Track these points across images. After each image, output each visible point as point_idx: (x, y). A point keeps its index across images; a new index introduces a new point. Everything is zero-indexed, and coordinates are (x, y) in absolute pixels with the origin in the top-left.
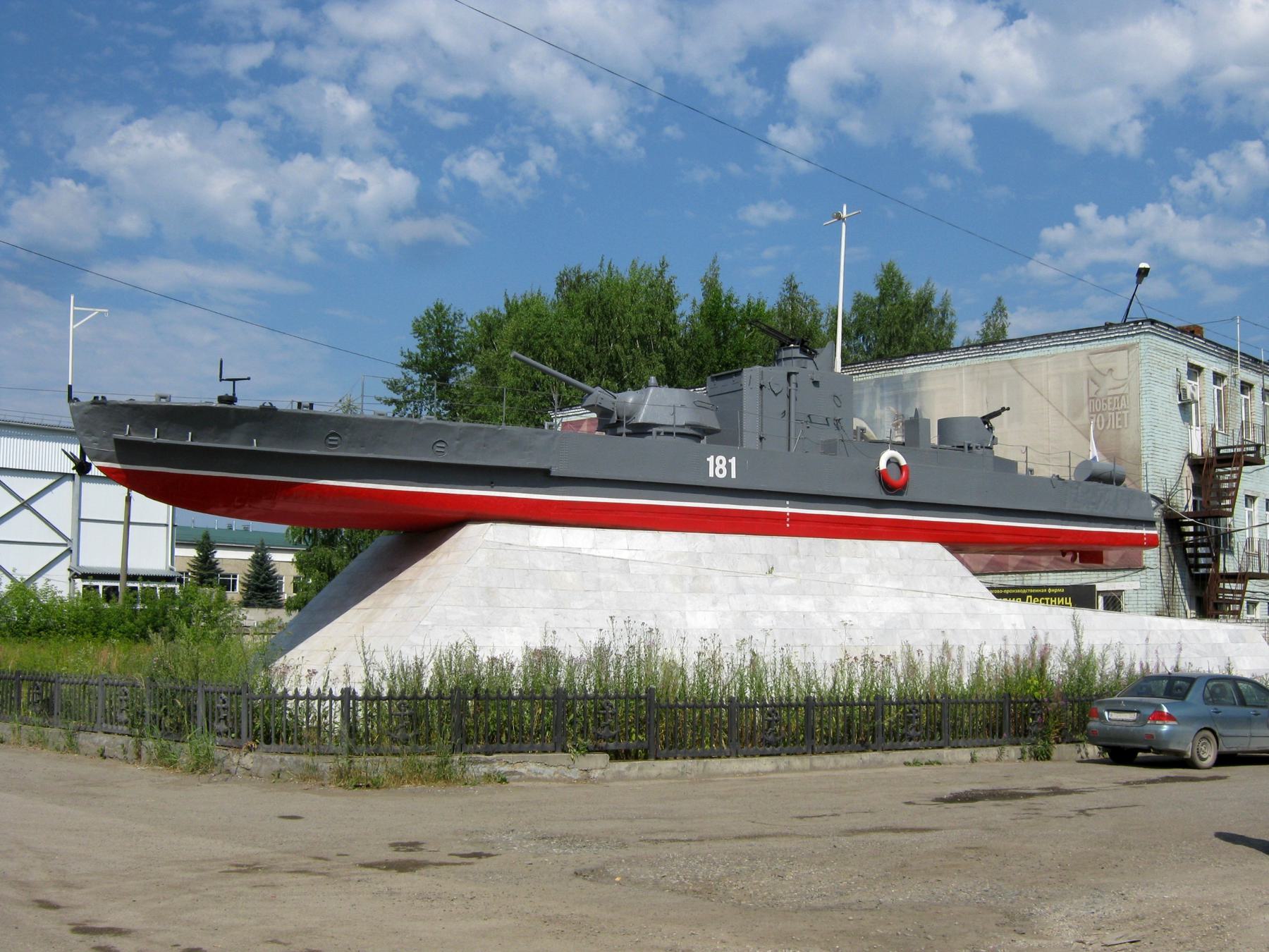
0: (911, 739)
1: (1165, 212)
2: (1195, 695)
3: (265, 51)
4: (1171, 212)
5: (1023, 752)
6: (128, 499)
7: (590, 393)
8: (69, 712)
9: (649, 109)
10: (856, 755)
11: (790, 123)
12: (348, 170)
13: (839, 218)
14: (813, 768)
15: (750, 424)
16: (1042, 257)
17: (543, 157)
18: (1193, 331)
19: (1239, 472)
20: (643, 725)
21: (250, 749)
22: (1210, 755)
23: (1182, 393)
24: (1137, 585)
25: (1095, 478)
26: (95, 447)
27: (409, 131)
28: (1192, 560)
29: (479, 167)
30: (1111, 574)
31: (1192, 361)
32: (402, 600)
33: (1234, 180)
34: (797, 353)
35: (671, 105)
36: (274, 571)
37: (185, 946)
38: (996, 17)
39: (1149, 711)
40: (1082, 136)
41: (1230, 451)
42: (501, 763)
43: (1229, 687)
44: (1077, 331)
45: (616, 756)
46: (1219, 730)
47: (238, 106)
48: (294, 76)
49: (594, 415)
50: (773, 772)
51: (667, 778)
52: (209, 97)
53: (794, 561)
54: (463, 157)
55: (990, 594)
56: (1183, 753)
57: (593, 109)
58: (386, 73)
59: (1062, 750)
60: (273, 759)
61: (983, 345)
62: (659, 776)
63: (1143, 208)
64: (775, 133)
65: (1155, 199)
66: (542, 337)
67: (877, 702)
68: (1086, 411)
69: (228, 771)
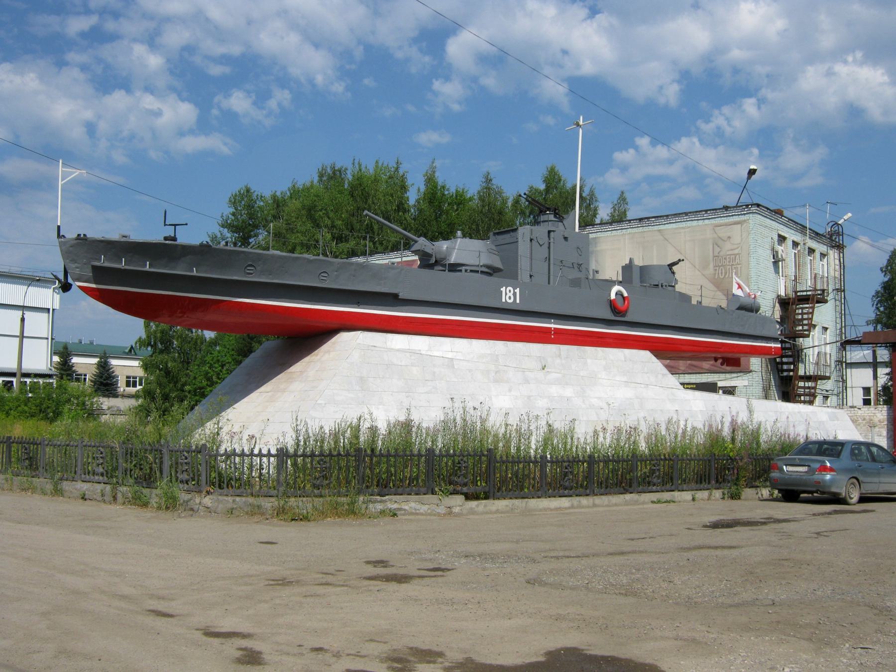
0: (654, 485)
1: (694, 143)
2: (846, 453)
3: (94, 20)
4: (697, 144)
5: (724, 494)
6: (23, 320)
7: (416, 242)
8: (50, 468)
9: (354, 67)
10: (622, 496)
11: (447, 79)
12: (149, 102)
13: (578, 125)
14: (595, 505)
15: (524, 264)
16: (615, 171)
17: (281, 97)
18: (779, 213)
19: (813, 308)
20: (488, 476)
21: (208, 493)
22: (855, 496)
23: (775, 255)
24: (746, 383)
25: (742, 308)
26: (77, 271)
27: (192, 78)
28: (780, 366)
29: (239, 102)
30: (728, 376)
31: (780, 233)
32: (297, 386)
33: (737, 123)
34: (552, 217)
35: (368, 65)
36: (113, 372)
37: (455, 656)
38: (584, 13)
39: (817, 465)
40: (640, 92)
41: (805, 293)
42: (392, 502)
43: (863, 449)
44: (706, 211)
45: (468, 497)
46: (861, 479)
47: (72, 56)
48: (113, 37)
49: (416, 258)
50: (569, 508)
51: (502, 512)
52: (52, 50)
53: (558, 361)
54: (228, 96)
55: (681, 387)
56: (839, 494)
57: (316, 65)
58: (176, 37)
59: (748, 492)
60: (229, 501)
61: (611, 224)
62: (497, 511)
63: (679, 140)
64: (437, 85)
65: (688, 134)
66: (321, 210)
67: (635, 458)
68: (711, 266)
69: (192, 509)
